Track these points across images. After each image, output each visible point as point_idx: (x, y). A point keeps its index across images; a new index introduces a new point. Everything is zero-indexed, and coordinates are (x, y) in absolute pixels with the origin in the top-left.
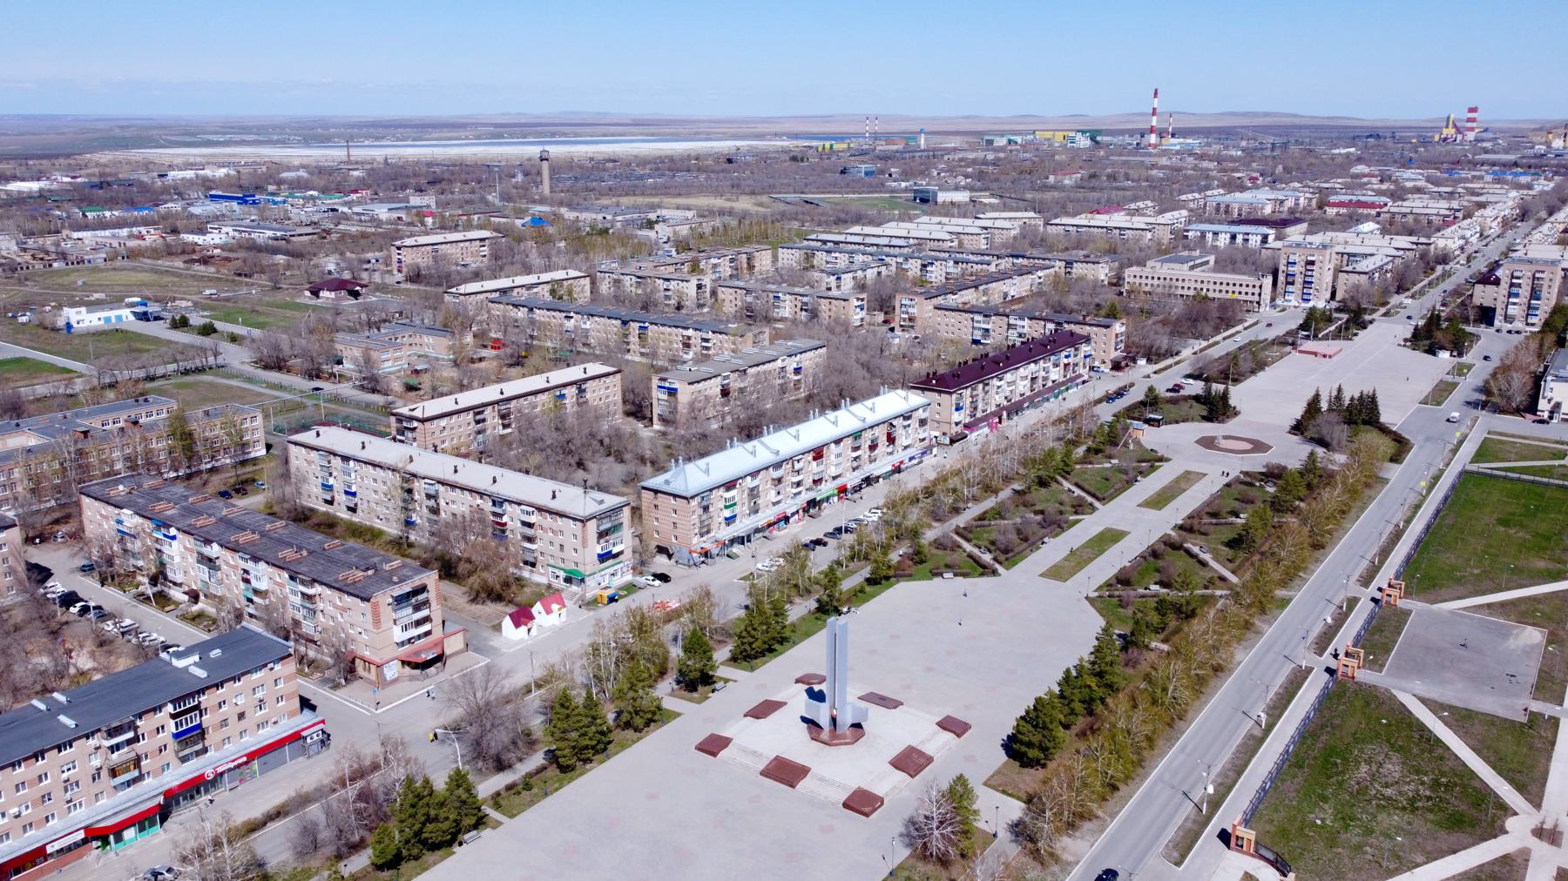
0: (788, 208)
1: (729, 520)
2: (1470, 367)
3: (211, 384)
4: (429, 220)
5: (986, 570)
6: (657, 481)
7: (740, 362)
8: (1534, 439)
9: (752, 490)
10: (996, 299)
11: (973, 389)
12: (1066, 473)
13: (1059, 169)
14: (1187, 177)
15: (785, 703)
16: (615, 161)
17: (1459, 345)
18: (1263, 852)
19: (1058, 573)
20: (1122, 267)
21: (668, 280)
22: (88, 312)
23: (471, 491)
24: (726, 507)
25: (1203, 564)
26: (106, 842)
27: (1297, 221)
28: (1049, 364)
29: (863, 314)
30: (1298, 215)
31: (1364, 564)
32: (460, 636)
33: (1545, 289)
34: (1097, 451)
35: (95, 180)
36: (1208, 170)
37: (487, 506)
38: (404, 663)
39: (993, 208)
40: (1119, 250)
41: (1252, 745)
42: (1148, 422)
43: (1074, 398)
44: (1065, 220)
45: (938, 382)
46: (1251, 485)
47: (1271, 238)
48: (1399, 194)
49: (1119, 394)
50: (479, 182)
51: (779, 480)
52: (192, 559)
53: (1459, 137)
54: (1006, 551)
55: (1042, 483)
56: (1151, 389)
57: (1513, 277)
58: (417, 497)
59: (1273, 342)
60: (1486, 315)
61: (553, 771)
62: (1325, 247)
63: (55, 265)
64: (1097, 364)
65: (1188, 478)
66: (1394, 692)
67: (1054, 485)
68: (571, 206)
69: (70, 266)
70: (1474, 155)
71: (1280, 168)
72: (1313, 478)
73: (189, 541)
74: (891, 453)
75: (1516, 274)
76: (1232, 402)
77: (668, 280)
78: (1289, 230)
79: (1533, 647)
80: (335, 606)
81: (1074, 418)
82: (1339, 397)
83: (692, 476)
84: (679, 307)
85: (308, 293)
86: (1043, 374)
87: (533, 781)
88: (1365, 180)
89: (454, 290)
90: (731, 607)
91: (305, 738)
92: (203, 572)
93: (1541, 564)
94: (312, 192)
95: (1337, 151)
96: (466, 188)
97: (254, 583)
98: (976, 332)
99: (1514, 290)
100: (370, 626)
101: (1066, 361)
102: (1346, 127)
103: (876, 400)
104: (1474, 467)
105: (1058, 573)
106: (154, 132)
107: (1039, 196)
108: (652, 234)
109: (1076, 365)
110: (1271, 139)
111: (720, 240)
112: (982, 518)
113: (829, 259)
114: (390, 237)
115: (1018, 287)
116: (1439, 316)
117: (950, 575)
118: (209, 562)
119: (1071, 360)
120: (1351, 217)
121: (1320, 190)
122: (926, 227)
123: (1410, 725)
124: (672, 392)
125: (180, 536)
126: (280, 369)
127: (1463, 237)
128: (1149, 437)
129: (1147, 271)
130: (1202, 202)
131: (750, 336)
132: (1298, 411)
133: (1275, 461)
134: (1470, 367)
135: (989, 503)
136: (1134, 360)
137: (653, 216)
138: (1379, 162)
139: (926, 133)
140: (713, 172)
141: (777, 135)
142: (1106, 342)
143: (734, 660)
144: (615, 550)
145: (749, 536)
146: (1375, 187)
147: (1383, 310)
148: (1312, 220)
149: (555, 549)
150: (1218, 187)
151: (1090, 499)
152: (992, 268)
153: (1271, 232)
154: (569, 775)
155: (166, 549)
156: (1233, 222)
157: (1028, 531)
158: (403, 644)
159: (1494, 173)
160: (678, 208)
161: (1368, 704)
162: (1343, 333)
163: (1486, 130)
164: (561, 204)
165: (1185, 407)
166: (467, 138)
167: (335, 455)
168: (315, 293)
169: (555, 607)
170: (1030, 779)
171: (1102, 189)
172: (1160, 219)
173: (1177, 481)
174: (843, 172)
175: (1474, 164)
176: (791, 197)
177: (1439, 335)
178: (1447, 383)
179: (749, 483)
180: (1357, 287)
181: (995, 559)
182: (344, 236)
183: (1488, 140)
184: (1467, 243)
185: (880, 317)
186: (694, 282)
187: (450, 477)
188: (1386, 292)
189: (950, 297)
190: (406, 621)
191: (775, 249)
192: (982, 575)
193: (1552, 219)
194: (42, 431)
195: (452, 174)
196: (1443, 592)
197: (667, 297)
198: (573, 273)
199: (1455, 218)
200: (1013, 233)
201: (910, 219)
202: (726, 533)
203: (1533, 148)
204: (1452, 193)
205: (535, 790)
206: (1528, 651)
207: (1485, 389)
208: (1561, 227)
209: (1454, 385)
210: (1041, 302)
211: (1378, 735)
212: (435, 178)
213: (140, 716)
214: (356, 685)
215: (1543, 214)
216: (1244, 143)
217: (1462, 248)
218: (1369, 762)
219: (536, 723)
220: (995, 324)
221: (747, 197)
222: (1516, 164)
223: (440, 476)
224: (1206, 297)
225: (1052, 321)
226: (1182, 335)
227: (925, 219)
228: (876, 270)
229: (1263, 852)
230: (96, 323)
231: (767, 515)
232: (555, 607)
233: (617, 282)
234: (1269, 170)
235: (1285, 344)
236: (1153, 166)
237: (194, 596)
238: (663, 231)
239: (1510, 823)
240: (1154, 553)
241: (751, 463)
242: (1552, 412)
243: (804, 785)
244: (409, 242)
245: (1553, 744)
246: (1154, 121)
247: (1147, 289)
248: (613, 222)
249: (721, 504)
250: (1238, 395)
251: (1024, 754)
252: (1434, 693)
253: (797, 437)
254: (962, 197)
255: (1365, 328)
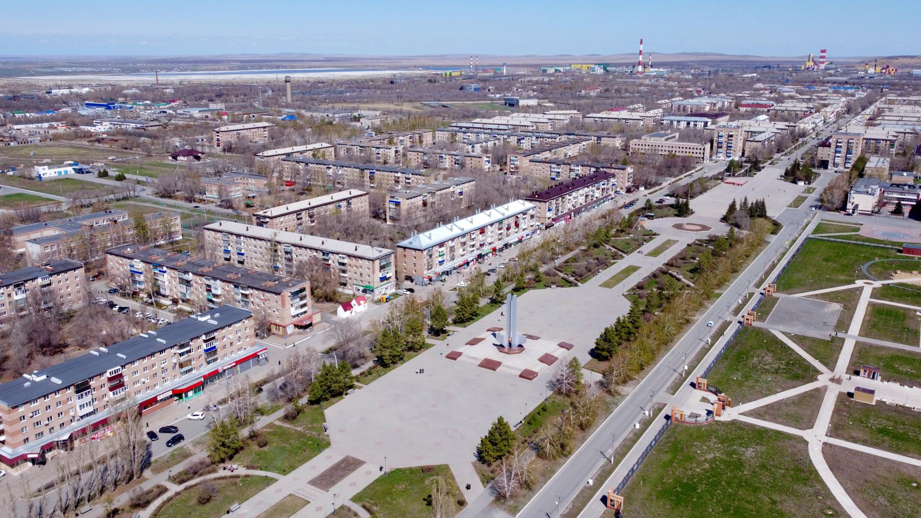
0: (432, 109)
1: (441, 263)
2: (814, 189)
3: (135, 205)
4: (225, 117)
5: (571, 284)
6: (404, 243)
7: (432, 188)
8: (844, 223)
9: (452, 248)
10: (562, 157)
11: (557, 200)
12: (607, 242)
13: (587, 86)
14: (661, 91)
15: (484, 339)
16: (323, 83)
17: (808, 179)
18: (711, 388)
19: (608, 285)
20: (628, 140)
21: (378, 148)
22: (49, 168)
23: (311, 249)
24: (440, 256)
25: (679, 280)
26: (181, 397)
27: (723, 115)
28: (594, 188)
29: (489, 165)
30: (724, 112)
31: (757, 279)
32: (319, 314)
33: (854, 148)
34: (622, 231)
35: (10, 95)
36: (672, 86)
37: (320, 255)
38: (296, 326)
39: (553, 109)
40: (626, 131)
41: (704, 351)
42: (647, 217)
43: (608, 205)
44: (594, 115)
45: (534, 197)
46: (702, 245)
47: (709, 124)
48: (780, 100)
49: (631, 204)
50: (245, 95)
51: (464, 243)
52: (175, 283)
53: (816, 67)
54: (581, 276)
55: (596, 246)
56: (648, 201)
57: (837, 142)
58: (279, 253)
59: (711, 178)
60: (824, 164)
61: (379, 368)
62: (738, 127)
63: (12, 144)
64: (618, 189)
65: (669, 243)
66: (770, 330)
67: (601, 247)
68: (309, 110)
69: (20, 145)
70: (824, 77)
71: (714, 85)
72: (732, 241)
73: (176, 274)
74: (517, 232)
75: (839, 141)
76: (690, 207)
77: (378, 148)
78: (719, 119)
79: (836, 311)
80: (261, 299)
81: (609, 215)
82: (745, 203)
83: (424, 239)
84: (385, 163)
85: (170, 158)
86: (591, 193)
87: (372, 371)
88: (762, 92)
89: (261, 154)
90: (450, 301)
91: (259, 356)
92: (183, 288)
93: (843, 277)
94: (147, 102)
95: (746, 76)
96: (238, 98)
97: (214, 291)
98: (553, 174)
99: (838, 149)
100: (280, 308)
101: (603, 187)
102: (752, 62)
103: (474, 217)
104: (813, 236)
105: (608, 285)
106: (27, 66)
107: (577, 102)
108: (358, 124)
109: (608, 189)
110: (707, 69)
111: (400, 127)
112: (567, 262)
113: (465, 137)
114: (205, 127)
115: (572, 151)
116: (799, 165)
117: (555, 286)
118: (188, 283)
119: (605, 186)
120: (753, 113)
121: (736, 98)
122: (516, 119)
123: (777, 342)
124: (398, 204)
125: (168, 271)
126: (170, 197)
127: (814, 123)
128: (648, 224)
129: (642, 141)
130: (670, 105)
131: (433, 176)
132: (724, 211)
133: (713, 234)
134: (814, 189)
135: (570, 255)
136: (638, 188)
137: (356, 114)
138: (769, 82)
139: (507, 66)
140: (384, 89)
141: (416, 67)
142: (623, 177)
143: (455, 322)
144: (388, 276)
145: (451, 271)
146: (767, 96)
147: (770, 162)
148: (732, 114)
149: (358, 276)
150: (679, 96)
151: (620, 253)
152: (557, 140)
153: (709, 121)
154: (388, 369)
155: (160, 278)
156: (688, 115)
157: (592, 267)
158: (294, 317)
159: (834, 88)
160: (369, 109)
161: (758, 335)
162: (748, 173)
163: (831, 63)
164: (300, 108)
165: (666, 210)
166: (224, 69)
167: (232, 234)
168: (175, 158)
169: (362, 302)
170: (604, 365)
171: (612, 98)
172: (648, 114)
173: (664, 244)
174: (461, 89)
175: (823, 83)
176: (433, 103)
177: (798, 173)
178: (802, 197)
179: (450, 244)
180: (755, 149)
181: (576, 279)
182: (177, 127)
183: (833, 69)
184: (816, 126)
185: (498, 168)
186: (393, 149)
187: (298, 242)
188: (771, 152)
189: (537, 155)
190: (296, 305)
191: (434, 131)
192: (570, 286)
193: (863, 113)
194: (61, 227)
195: (227, 90)
196: (794, 290)
197: (379, 158)
198: (325, 145)
199: (811, 112)
200: (566, 122)
201: (506, 115)
202: (440, 269)
203: (857, 73)
204: (810, 99)
205: (374, 375)
206: (833, 313)
207: (821, 200)
208: (868, 117)
209: (806, 198)
210: (586, 158)
211: (762, 346)
212: (220, 93)
213: (192, 340)
214: (272, 337)
215: (859, 110)
216: (692, 71)
217: (813, 129)
218: (758, 357)
219: (366, 351)
220: (563, 169)
221: (408, 103)
222: (846, 83)
223: (293, 242)
224: (674, 155)
225: (594, 167)
226: (662, 175)
227: (515, 114)
228: (493, 142)
229: (711, 388)
230: (53, 175)
231: (459, 261)
232: (362, 302)
233: (348, 150)
234: (707, 86)
235: (718, 179)
236: (641, 85)
237: (175, 302)
238: (365, 123)
239: (819, 377)
240: (654, 275)
241: (451, 234)
242: (854, 210)
243: (499, 369)
244: (223, 129)
245: (841, 348)
246: (641, 58)
247: (643, 151)
248: (334, 119)
249: (437, 255)
250: (693, 204)
251: (600, 354)
252: (788, 330)
253: (471, 222)
254: (533, 102)
255: (760, 170)
